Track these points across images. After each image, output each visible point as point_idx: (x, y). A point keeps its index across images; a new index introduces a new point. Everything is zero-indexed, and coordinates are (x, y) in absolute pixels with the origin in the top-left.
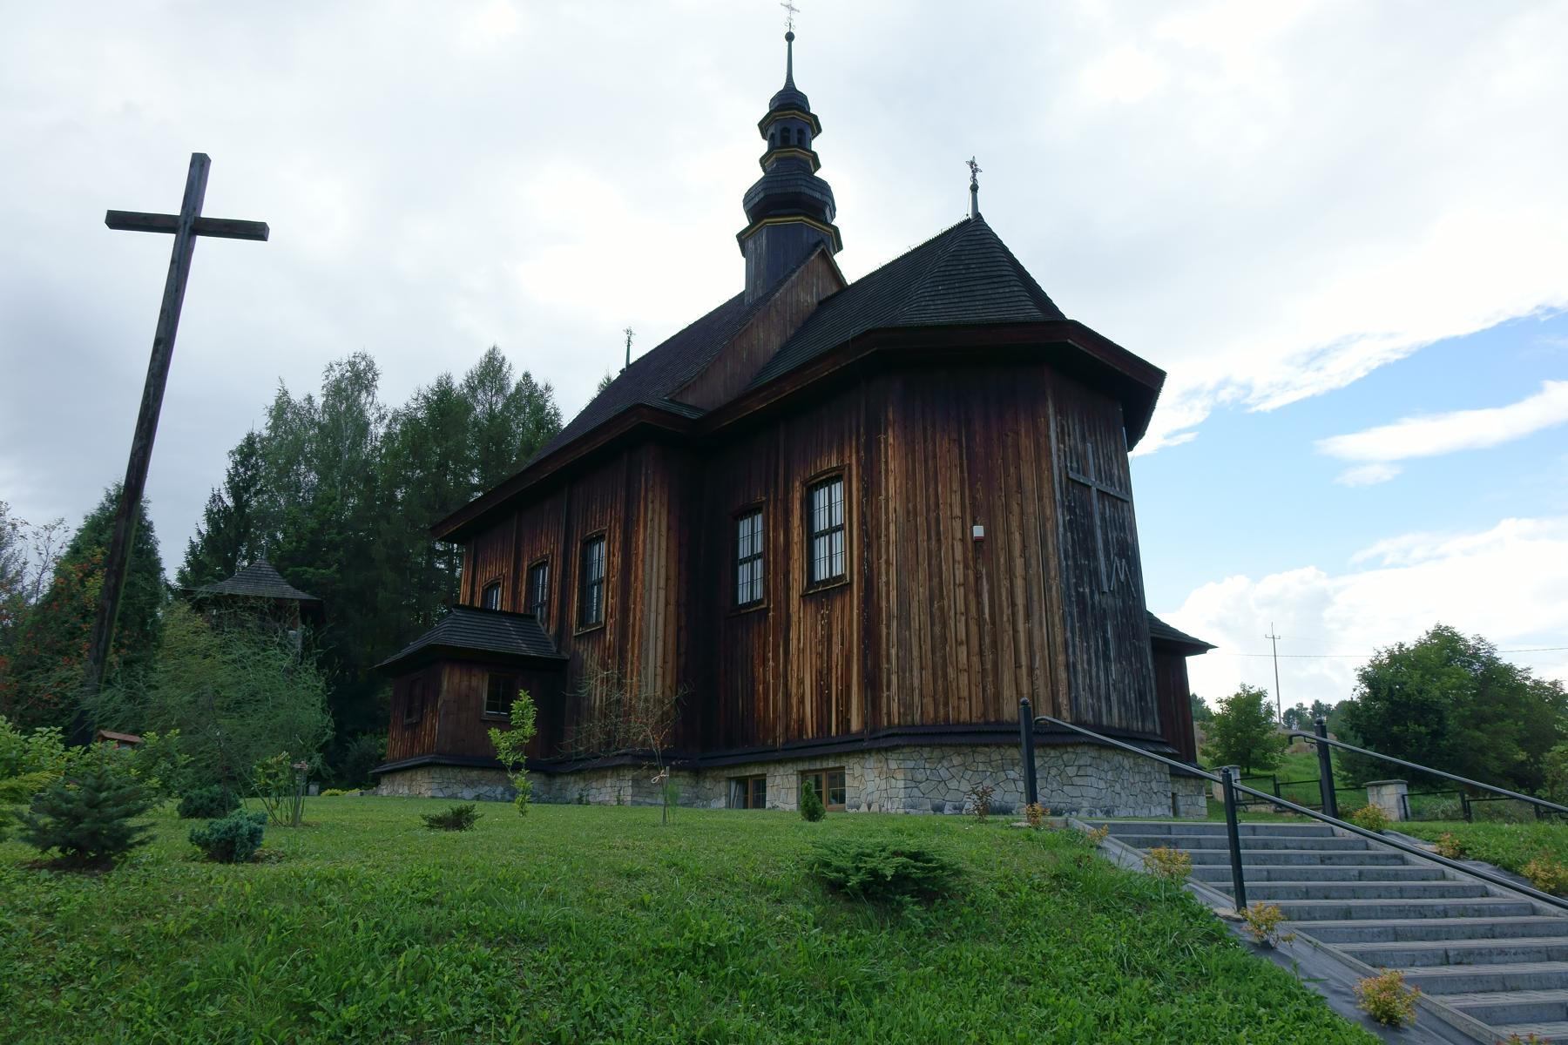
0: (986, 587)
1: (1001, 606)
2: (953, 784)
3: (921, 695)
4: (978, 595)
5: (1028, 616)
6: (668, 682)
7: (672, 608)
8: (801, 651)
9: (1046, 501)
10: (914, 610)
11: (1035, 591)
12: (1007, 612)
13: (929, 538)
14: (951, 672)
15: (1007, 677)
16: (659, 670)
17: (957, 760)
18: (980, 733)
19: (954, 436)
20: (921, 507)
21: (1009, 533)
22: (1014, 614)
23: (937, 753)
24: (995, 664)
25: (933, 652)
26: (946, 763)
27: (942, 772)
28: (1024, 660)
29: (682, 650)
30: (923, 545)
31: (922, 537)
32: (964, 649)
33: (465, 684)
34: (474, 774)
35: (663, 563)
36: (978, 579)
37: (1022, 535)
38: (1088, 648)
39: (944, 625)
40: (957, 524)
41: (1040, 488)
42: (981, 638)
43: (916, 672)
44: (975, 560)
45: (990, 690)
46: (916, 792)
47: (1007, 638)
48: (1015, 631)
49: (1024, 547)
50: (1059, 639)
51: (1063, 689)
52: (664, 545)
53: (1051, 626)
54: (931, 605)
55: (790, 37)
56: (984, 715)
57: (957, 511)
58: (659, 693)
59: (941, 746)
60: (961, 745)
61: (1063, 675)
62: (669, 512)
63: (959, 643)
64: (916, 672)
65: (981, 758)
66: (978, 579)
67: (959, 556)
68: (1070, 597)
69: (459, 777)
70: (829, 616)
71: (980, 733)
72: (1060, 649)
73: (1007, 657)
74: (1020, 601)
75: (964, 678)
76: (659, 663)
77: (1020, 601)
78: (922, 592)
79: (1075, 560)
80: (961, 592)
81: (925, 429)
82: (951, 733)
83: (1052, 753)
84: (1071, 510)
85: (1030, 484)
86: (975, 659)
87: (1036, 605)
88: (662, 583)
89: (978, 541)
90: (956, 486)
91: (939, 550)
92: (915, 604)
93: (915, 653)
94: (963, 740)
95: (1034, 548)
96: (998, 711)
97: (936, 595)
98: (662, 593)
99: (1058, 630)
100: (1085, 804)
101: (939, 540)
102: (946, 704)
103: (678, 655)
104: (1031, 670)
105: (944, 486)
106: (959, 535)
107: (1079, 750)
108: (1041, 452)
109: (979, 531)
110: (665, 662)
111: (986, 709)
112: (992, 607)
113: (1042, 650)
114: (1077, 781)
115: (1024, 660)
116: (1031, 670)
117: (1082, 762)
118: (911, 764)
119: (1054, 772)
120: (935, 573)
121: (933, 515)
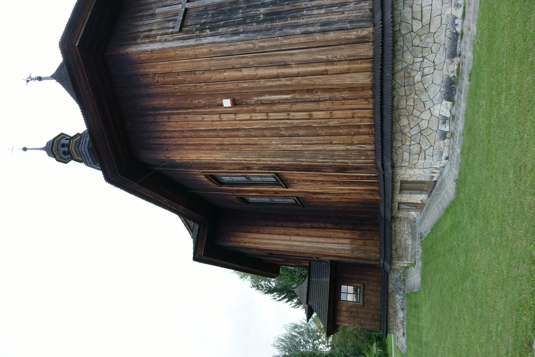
0: (267, 97)
1: (279, 86)
2: (424, 124)
3: (352, 144)
4: (273, 103)
5: (286, 65)
6: (341, 235)
7: (301, 232)
8: (321, 189)
9: (198, 51)
10: (289, 147)
11: (265, 59)
12: (284, 81)
13: (237, 136)
14: (333, 123)
15: (335, 81)
16: (335, 241)
17: (404, 122)
18: (382, 102)
19: (166, 118)
20: (217, 141)
21: (224, 81)
22: (285, 76)
23: (398, 136)
24: (324, 90)
25: (318, 135)
26: (407, 130)
27: (413, 132)
28: (322, 68)
29: (323, 225)
30: (242, 140)
31: (236, 140)
32: (314, 113)
33: (345, 314)
34: (391, 311)
35: (276, 237)
36: (262, 104)
37: (225, 70)
38: (308, 9)
39: (298, 127)
40: (225, 117)
41: (189, 57)
42: (306, 101)
43: (335, 148)
44: (248, 105)
45: (345, 94)
46: (429, 152)
47: (304, 81)
48: (298, 75)
49: (233, 68)
50: (303, 39)
51: (343, 35)
52: (267, 236)
53: (292, 48)
54: (284, 136)
55: (25, 149)
56: (366, 99)
57: (216, 117)
58: (348, 241)
59: (392, 133)
60: (392, 119)
61: (331, 36)
62: (250, 232)
63: (311, 117)
64: (335, 148)
65: (403, 103)
66: (262, 104)
67: (246, 116)
68: (267, 30)
69: (392, 319)
70: (297, 180)
71: (382, 102)
72: (310, 38)
73: (319, 80)
74: (275, 71)
75: (338, 114)
76: (331, 240)
77: (275, 71)
78: (275, 141)
79: (239, 24)
80: (272, 115)
81: (165, 137)
82: (382, 126)
83: (400, 43)
84: (202, 30)
85: (188, 65)
86: (322, 105)
87: (277, 59)
88: (287, 238)
89: (234, 103)
90: (199, 118)
91: (245, 129)
92: (285, 147)
93: (320, 148)
94: (387, 115)
95: (233, 61)
96: (363, 88)
97: (276, 132)
98: (293, 238)
99: (295, 40)
100: (448, 12)
101: (238, 130)
102: (359, 127)
103: (326, 228)
104: (329, 62)
105: (200, 125)
106: (232, 116)
107: (398, 20)
108: (164, 56)
109: (227, 103)
110: (330, 237)
111: (362, 98)
112: (282, 93)
113: (312, 53)
114: (426, 20)
115: (322, 68)
116: (329, 62)
117: (409, 17)
118: (406, 155)
119: (417, 42)
120: (262, 132)
121: (221, 133)
